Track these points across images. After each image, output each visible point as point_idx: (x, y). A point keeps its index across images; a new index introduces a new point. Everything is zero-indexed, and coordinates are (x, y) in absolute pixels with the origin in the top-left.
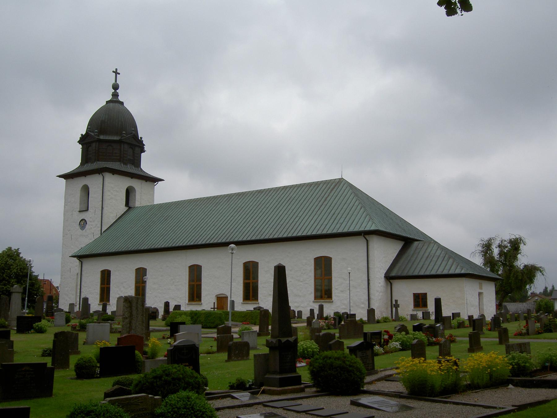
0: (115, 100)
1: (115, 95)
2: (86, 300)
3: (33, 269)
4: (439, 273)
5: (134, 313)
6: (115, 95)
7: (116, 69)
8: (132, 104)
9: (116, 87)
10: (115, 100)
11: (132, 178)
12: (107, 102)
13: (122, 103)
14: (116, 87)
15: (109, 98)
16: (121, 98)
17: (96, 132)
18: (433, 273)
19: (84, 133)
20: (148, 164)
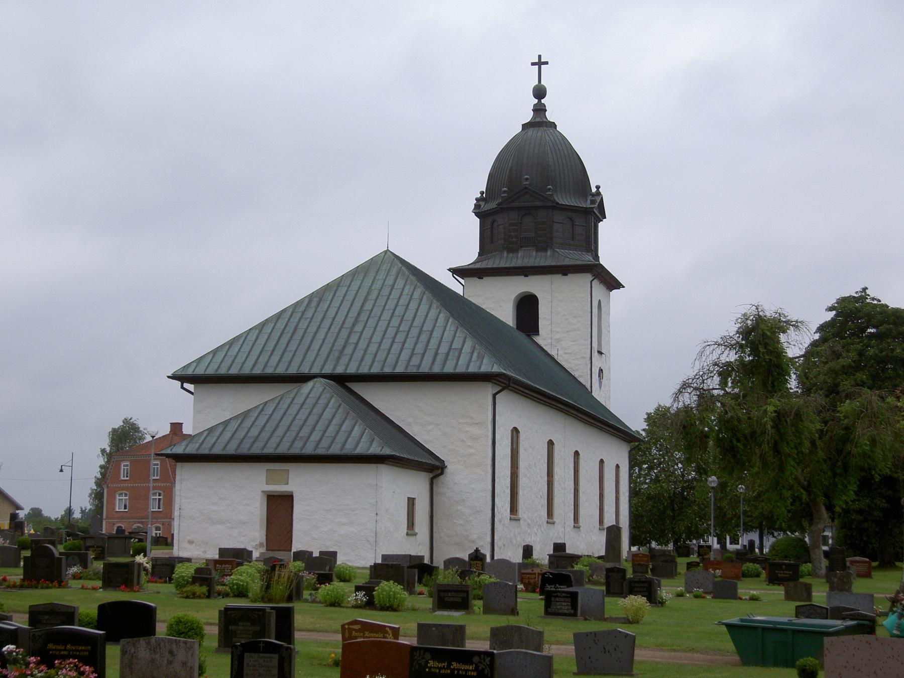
0: (539, 121)
1: (540, 110)
2: (10, 618)
3: (54, 512)
4: (321, 451)
5: (678, 654)
6: (540, 110)
7: (546, 63)
8: (570, 121)
9: (540, 93)
10: (539, 121)
11: (526, 276)
12: (525, 126)
13: (553, 125)
14: (540, 93)
15: (528, 116)
16: (550, 116)
17: (505, 192)
18: (335, 450)
19: (601, 225)
20: (613, 245)
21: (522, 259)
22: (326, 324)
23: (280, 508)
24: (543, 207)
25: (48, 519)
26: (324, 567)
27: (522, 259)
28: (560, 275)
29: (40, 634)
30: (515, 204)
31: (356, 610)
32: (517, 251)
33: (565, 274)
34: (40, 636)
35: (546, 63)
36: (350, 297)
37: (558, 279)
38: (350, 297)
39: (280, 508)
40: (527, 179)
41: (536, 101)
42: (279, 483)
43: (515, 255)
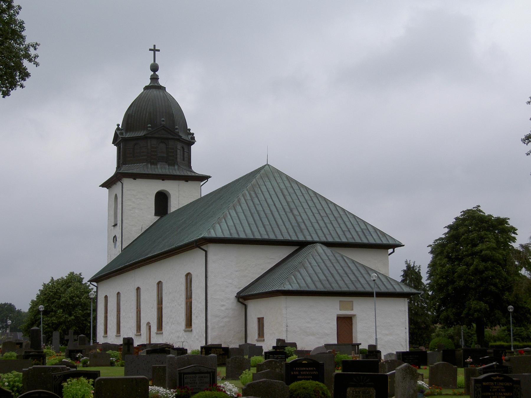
0: (154, 85)
1: (154, 78)
6: (154, 78)
9: (155, 68)
10: (154, 85)
11: (163, 180)
12: (146, 88)
14: (155, 68)
15: (148, 82)
16: (162, 82)
21: (160, 169)
22: (273, 208)
23: (345, 323)
24: (172, 139)
25: (19, 312)
26: (284, 349)
27: (160, 169)
28: (184, 182)
29: (59, 375)
30: (156, 135)
31: (155, 355)
32: (156, 164)
33: (187, 181)
34: (59, 377)
35: (159, 51)
36: (272, 192)
37: (182, 183)
38: (272, 192)
39: (345, 323)
40: (163, 121)
41: (152, 73)
42: (347, 309)
43: (155, 167)
